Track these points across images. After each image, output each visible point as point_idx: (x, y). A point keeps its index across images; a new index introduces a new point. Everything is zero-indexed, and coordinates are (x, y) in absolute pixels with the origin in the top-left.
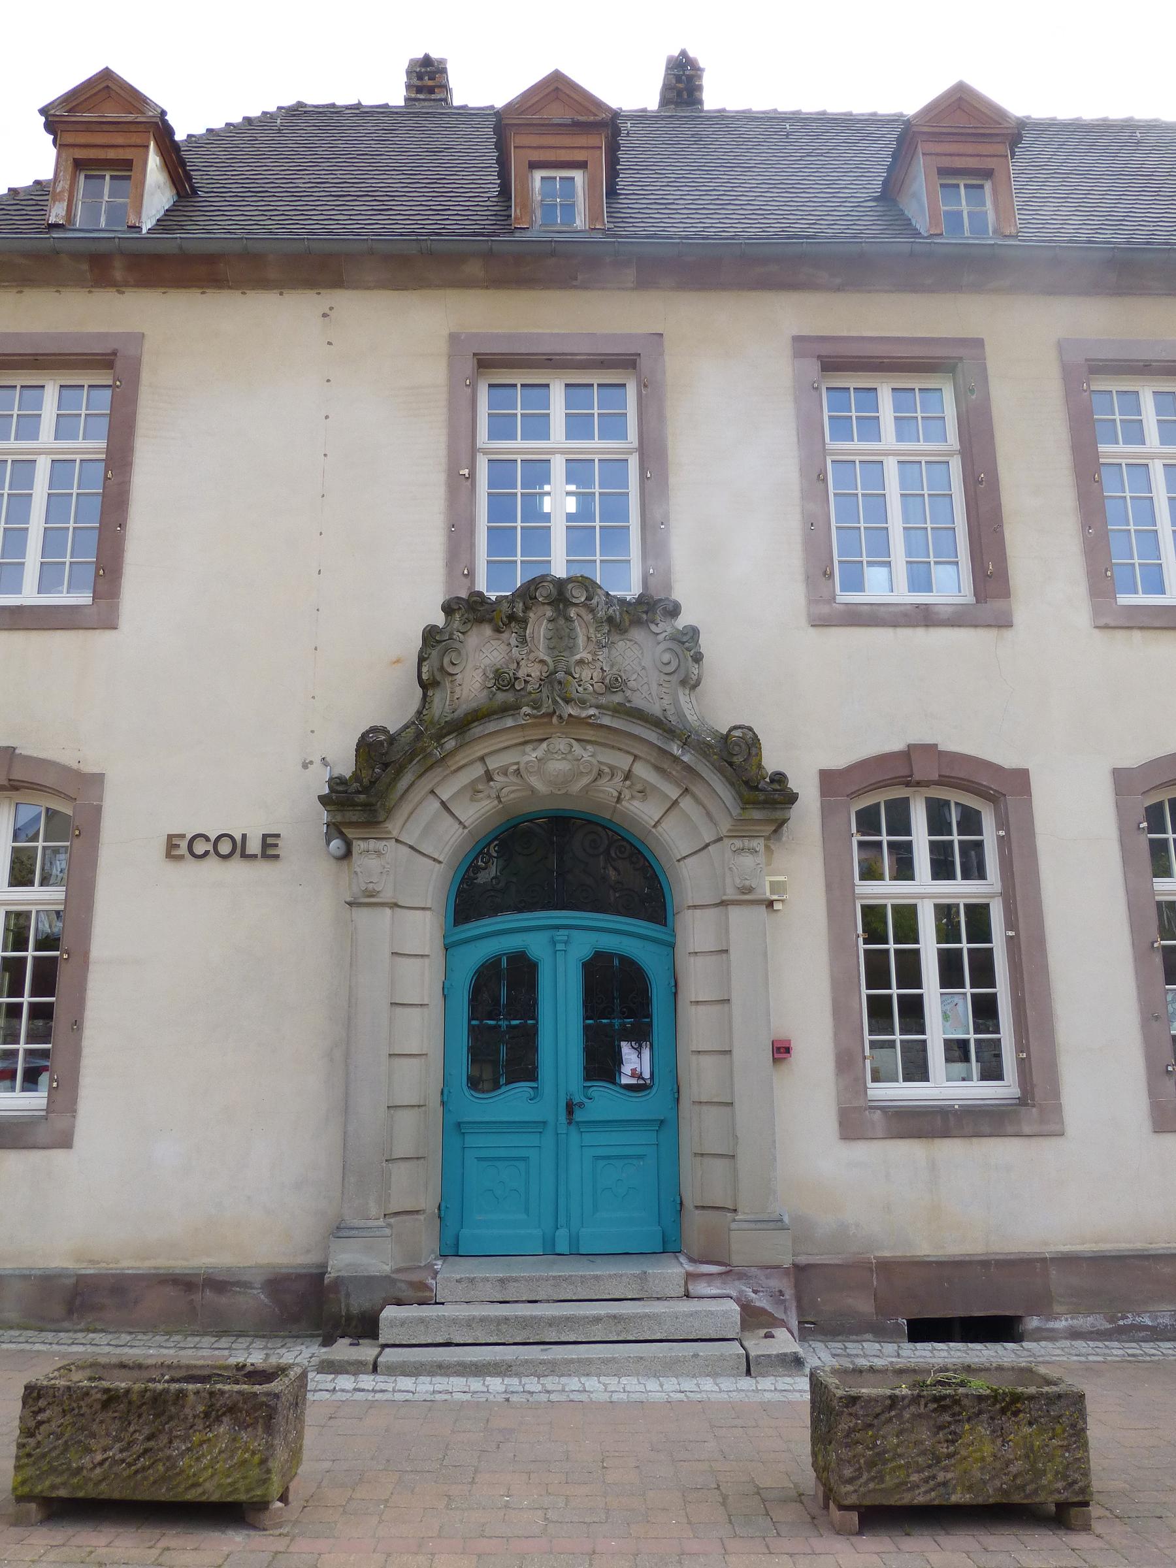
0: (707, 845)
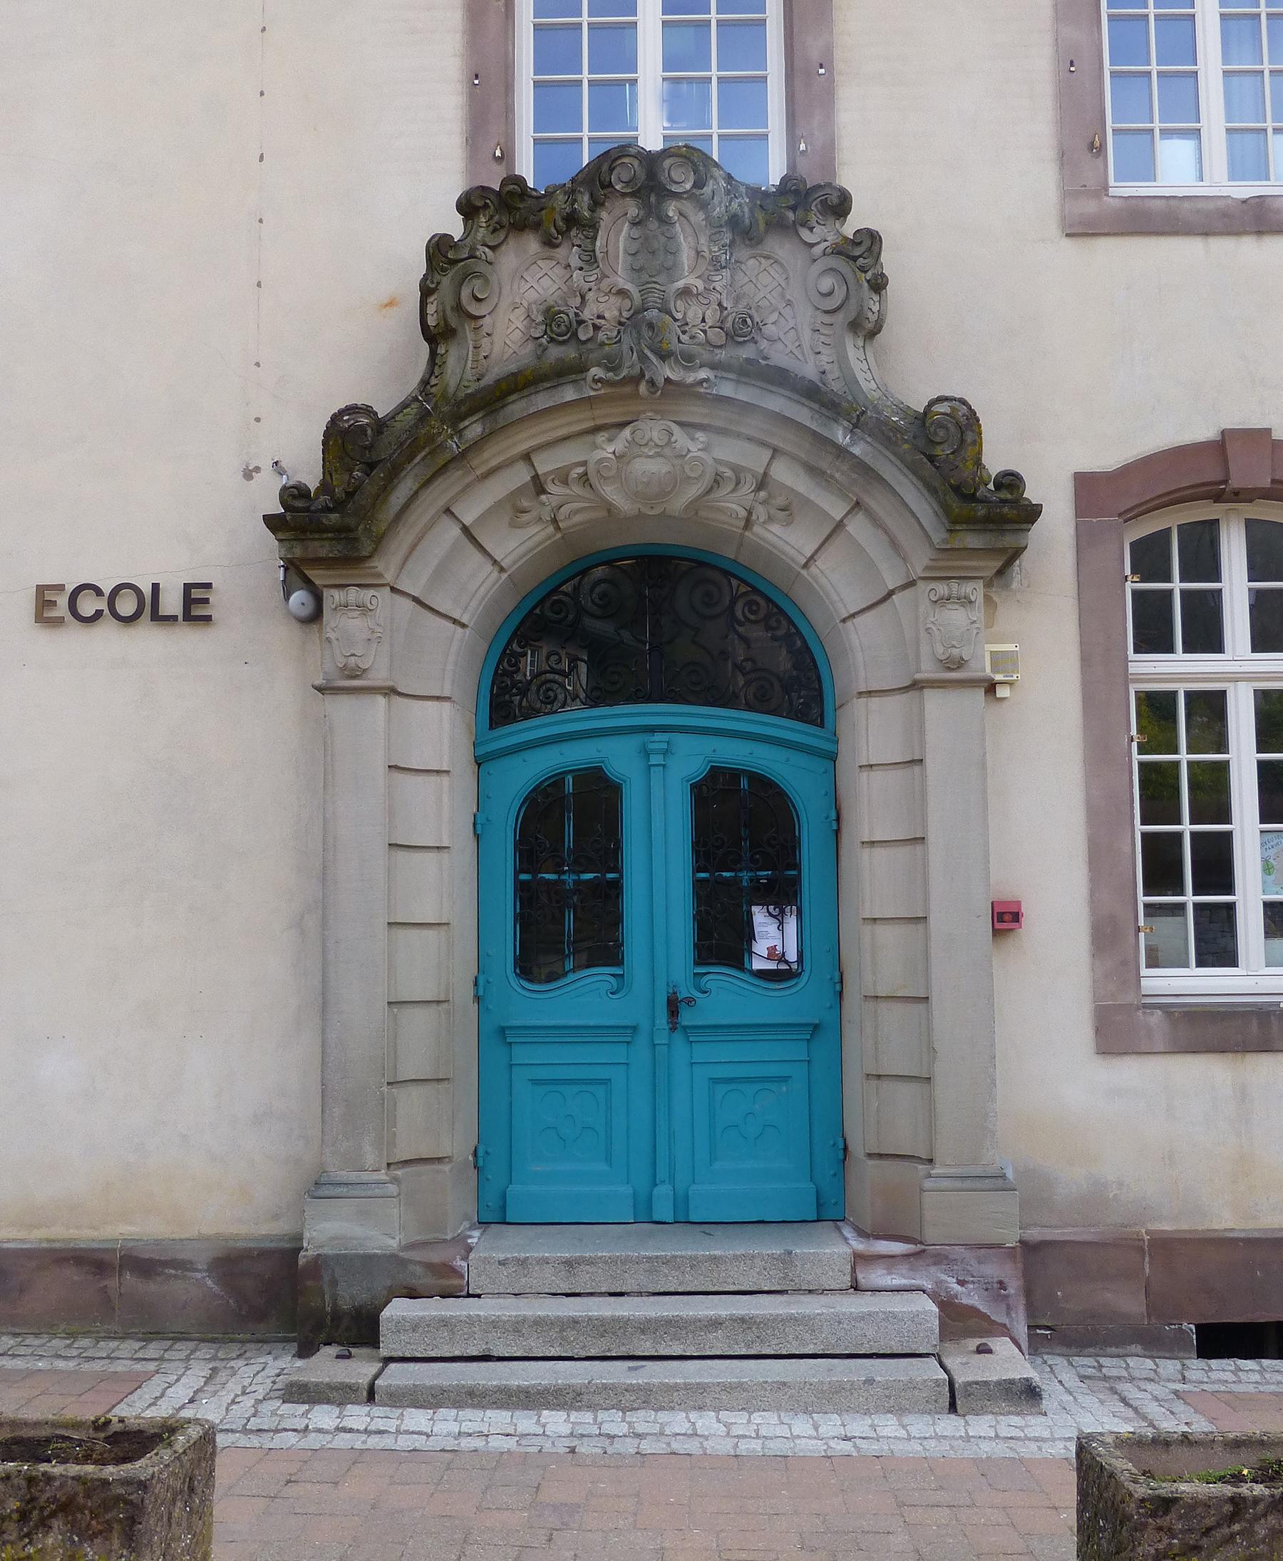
0: (891, 593)
